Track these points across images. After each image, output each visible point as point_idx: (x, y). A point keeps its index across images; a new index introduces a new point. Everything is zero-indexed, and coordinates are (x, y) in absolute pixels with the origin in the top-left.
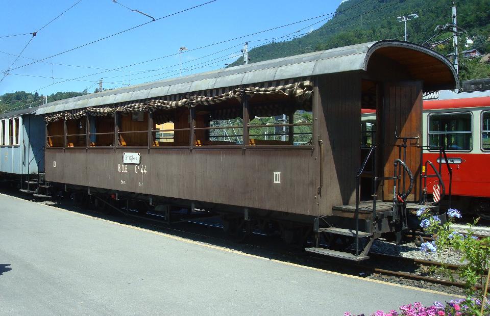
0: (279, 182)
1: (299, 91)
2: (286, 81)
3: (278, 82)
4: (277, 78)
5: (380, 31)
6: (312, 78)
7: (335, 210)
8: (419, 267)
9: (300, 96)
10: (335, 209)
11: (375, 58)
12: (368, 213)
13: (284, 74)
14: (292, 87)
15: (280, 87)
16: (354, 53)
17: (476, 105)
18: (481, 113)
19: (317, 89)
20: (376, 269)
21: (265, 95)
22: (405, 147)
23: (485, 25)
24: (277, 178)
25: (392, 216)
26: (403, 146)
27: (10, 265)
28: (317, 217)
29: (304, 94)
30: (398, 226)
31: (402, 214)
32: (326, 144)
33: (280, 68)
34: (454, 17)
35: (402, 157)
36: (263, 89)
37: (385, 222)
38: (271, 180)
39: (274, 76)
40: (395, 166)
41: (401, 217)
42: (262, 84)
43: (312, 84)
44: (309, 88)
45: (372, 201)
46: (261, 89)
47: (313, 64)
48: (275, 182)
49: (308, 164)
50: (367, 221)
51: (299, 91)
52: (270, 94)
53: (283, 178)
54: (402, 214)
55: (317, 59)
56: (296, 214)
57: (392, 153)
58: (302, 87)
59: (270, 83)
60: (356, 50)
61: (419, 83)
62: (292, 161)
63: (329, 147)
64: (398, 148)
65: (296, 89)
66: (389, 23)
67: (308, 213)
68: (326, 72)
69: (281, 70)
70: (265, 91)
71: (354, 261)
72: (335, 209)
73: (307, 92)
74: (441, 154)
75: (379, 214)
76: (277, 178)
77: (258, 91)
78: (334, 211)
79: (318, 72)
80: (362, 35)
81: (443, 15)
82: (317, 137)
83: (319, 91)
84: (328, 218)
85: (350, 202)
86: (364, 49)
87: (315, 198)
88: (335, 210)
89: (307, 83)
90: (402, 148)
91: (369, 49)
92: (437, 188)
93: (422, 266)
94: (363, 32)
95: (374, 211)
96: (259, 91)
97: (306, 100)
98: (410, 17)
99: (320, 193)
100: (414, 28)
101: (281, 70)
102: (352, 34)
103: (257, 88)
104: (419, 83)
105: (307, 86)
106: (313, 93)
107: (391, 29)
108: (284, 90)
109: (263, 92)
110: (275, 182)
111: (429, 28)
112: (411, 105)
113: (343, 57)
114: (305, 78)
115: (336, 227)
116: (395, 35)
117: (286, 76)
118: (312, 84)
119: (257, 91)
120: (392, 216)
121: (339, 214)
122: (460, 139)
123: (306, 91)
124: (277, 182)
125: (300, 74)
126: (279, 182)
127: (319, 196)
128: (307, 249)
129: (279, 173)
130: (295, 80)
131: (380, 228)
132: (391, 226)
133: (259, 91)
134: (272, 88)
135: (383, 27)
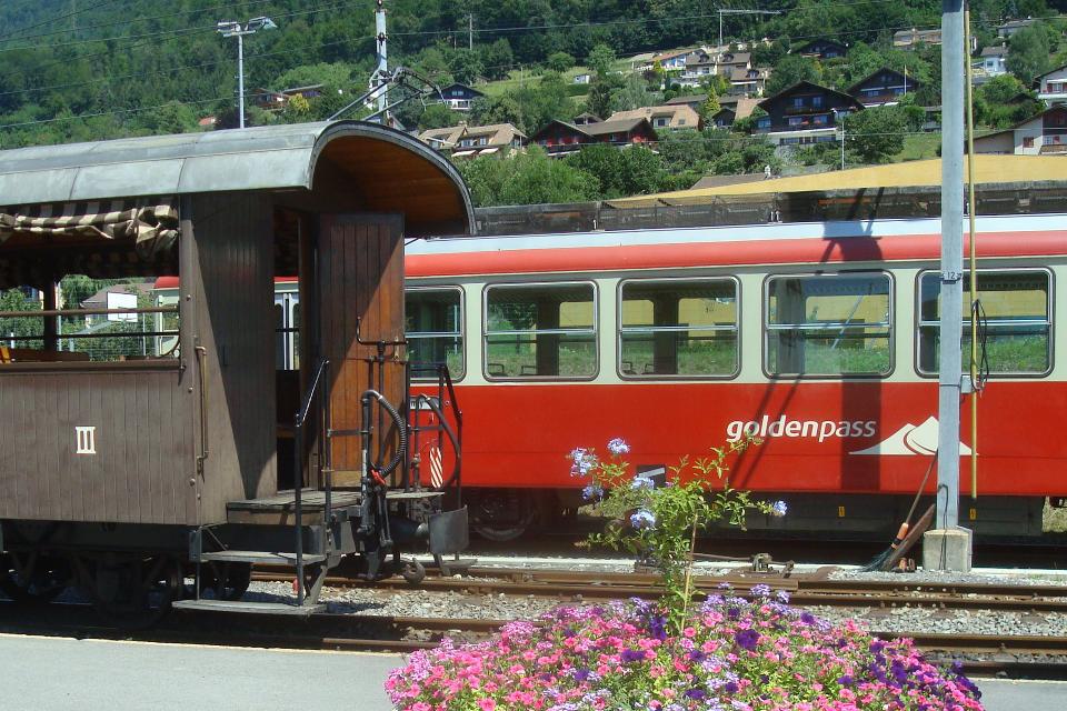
0: (92, 451)
1: (144, 231)
2: (105, 205)
3: (81, 207)
4: (79, 195)
5: (129, 48)
6: (176, 200)
7: (231, 509)
8: (405, 633)
9: (147, 242)
10: (230, 508)
11: (332, 161)
12: (315, 509)
13: (101, 186)
14: (121, 220)
15: (88, 219)
16: (278, 145)
17: (751, 259)
18: (484, 289)
19: (188, 227)
20: (325, 639)
21: (47, 237)
22: (381, 363)
23: (418, 50)
24: (86, 440)
25: (361, 518)
26: (376, 360)
27: (687, 325)
28: (196, 528)
29: (155, 238)
30: (370, 541)
31: (380, 512)
32: (211, 361)
33: (84, 172)
34: (381, 40)
35: (376, 383)
36: (41, 220)
37: (346, 528)
38: (68, 451)
39: (70, 188)
40: (364, 404)
41: (377, 518)
42: (34, 209)
43: (175, 214)
44: (169, 223)
45: (293, 491)
46: (34, 221)
47: (176, 166)
48: (79, 451)
49: (168, 406)
50: (314, 528)
51: (144, 231)
52: (60, 234)
53: (101, 441)
54: (380, 512)
55: (184, 154)
56: (141, 525)
57: (340, 379)
58: (149, 219)
59: (58, 208)
60: (287, 140)
61: (397, 220)
62: (123, 398)
63: (216, 361)
64: (367, 365)
65: (136, 225)
66: (155, 26)
67: (173, 520)
68: (214, 187)
69: (89, 178)
70: (44, 226)
71: (295, 616)
72: (230, 508)
73: (163, 233)
74: (441, 386)
75: (336, 512)
76: (86, 440)
77: (26, 225)
78: (230, 512)
79: (191, 185)
80: (75, 55)
81: (304, 13)
82: (192, 342)
83: (194, 230)
84: (219, 529)
85: (258, 494)
86: (306, 139)
87: (192, 484)
88: (231, 509)
89: (163, 211)
90: (376, 365)
91: (317, 140)
92: (436, 455)
93: (412, 630)
94: (79, 46)
95: (326, 506)
96: (31, 225)
97: (161, 254)
98: (253, 25)
99: (201, 471)
100: (225, 46)
101: (89, 178)
102: (44, 47)
103: (21, 218)
104: (397, 220)
105: (162, 218)
106: (179, 235)
107: (159, 42)
108: (100, 225)
109: (40, 229)
110: (79, 451)
111: (268, 48)
112: (380, 268)
113: (255, 156)
114: (156, 200)
115: (231, 548)
116: (172, 60)
117: (107, 191)
118: (175, 214)
119: (23, 224)
120: (361, 518)
121: (242, 519)
122: (424, 352)
123: (161, 229)
124: (86, 451)
125: (144, 188)
126: (92, 451)
127: (200, 477)
128: (176, 604)
129: (92, 429)
130: (128, 202)
131: (338, 546)
132: (357, 537)
133: (31, 225)
134: (65, 219)
135: (136, 34)
